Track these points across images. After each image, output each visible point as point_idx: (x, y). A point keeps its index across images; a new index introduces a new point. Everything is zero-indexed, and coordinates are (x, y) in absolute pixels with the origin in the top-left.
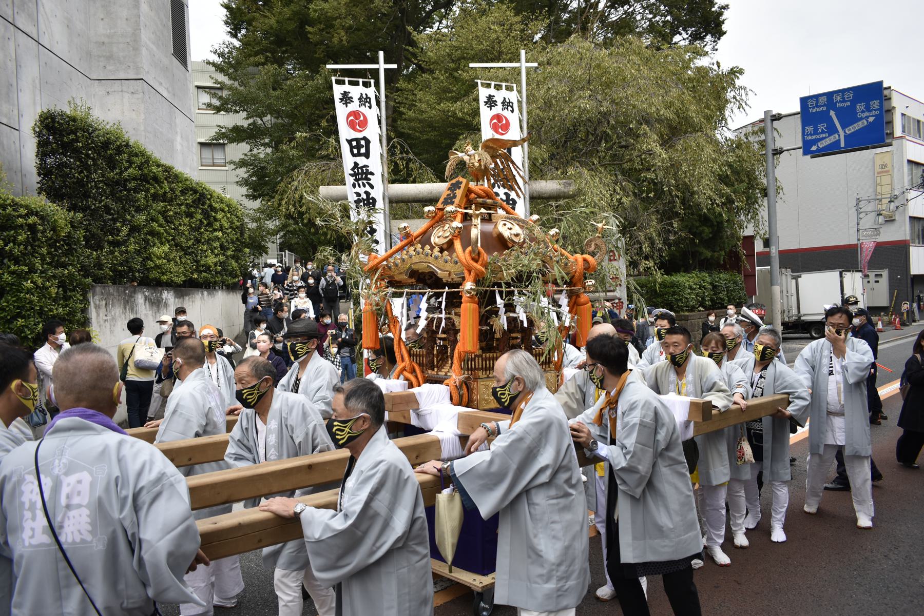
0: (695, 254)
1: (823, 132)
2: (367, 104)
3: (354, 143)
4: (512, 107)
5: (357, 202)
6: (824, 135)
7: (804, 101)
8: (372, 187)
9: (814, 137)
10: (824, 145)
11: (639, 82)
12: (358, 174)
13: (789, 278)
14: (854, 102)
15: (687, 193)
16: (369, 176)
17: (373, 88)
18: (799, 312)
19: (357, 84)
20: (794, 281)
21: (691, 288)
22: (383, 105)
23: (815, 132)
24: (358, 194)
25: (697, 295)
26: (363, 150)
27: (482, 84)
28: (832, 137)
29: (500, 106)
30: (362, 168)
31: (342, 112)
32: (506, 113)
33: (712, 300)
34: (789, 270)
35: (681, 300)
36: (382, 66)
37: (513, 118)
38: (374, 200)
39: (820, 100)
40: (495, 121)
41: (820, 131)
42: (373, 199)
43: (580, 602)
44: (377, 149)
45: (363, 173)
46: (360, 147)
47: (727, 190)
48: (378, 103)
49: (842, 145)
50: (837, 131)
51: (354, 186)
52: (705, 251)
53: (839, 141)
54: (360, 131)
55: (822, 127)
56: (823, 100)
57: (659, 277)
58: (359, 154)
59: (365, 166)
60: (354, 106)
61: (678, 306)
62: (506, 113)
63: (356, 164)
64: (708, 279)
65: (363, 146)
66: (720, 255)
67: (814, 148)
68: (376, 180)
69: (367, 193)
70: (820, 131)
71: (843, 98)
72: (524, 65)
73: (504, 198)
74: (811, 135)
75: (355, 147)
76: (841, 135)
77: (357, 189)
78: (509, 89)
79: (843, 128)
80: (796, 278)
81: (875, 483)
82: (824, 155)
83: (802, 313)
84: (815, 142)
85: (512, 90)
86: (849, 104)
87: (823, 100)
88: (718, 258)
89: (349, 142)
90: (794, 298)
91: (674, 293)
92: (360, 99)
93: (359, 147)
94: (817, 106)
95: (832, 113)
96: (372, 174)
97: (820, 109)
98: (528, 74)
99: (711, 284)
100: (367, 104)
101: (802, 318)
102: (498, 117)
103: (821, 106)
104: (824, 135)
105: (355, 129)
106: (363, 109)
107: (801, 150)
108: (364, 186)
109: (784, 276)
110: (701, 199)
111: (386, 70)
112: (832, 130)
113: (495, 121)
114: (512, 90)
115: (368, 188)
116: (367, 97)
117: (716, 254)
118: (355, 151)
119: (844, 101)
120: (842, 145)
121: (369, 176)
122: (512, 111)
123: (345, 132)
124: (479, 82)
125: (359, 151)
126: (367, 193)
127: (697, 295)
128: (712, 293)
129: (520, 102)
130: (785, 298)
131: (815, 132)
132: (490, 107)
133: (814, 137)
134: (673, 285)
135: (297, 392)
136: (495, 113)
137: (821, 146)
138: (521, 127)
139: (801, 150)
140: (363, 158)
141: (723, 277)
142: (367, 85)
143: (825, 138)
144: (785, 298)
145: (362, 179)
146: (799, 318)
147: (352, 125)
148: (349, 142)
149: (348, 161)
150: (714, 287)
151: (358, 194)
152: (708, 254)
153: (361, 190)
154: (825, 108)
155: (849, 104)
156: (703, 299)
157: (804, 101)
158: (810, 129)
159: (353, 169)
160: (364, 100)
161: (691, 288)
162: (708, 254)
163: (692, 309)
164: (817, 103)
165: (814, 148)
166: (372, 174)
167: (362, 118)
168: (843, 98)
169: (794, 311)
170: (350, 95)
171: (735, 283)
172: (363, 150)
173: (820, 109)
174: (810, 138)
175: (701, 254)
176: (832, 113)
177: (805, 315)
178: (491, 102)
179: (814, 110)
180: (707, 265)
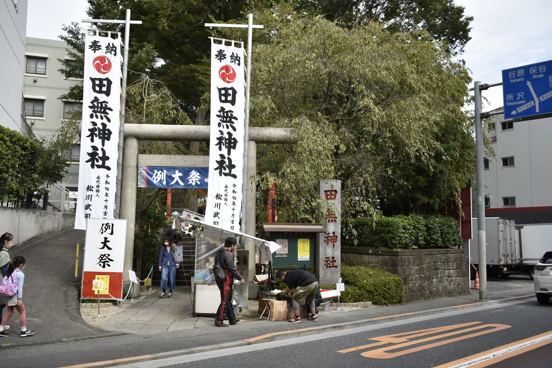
0: (414, 200)
1: (521, 99)
2: (113, 52)
3: (97, 82)
4: (239, 61)
6: (522, 102)
7: (505, 73)
9: (514, 103)
10: (522, 110)
11: (368, 48)
13: (513, 228)
14: (547, 74)
15: (399, 146)
16: (233, 120)
17: (120, 38)
18: (521, 256)
19: (106, 35)
20: (518, 231)
21: (404, 228)
22: (126, 53)
23: (515, 99)
24: (222, 133)
25: (411, 235)
26: (230, 98)
27: (214, 40)
28: (529, 104)
29: (104, 49)
30: (101, 103)
31: (216, 65)
32: (234, 66)
33: (425, 240)
34: (513, 222)
35: (395, 238)
36: (128, 22)
37: (239, 70)
39: (519, 72)
40: (224, 71)
41: (519, 98)
42: (234, 139)
44: (117, 90)
45: (102, 107)
46: (228, 95)
47: (438, 145)
48: (122, 53)
49: (537, 110)
50: (533, 99)
52: (422, 197)
53: (534, 107)
54: (104, 73)
55: (520, 95)
56: (521, 73)
57: (376, 216)
58: (226, 101)
59: (230, 111)
60: (227, 61)
61: (392, 244)
62: (234, 66)
63: (96, 99)
64: (423, 222)
65: (230, 95)
66: (436, 202)
67: (514, 113)
68: (239, 124)
69: (104, 125)
70: (519, 98)
71: (538, 71)
72: (251, 26)
73: (101, 127)
74: (511, 101)
76: (536, 102)
77: (94, 119)
78: (237, 45)
79: (538, 96)
80: (519, 228)
82: (524, 119)
83: (524, 257)
84: (515, 107)
85: (240, 47)
86: (542, 75)
87: (521, 73)
88: (434, 204)
89: (93, 80)
90: (517, 245)
91: (389, 232)
92: (107, 47)
93: (226, 95)
94: (516, 77)
95: (529, 84)
96: (236, 118)
97: (519, 80)
98: (253, 33)
99: (426, 226)
100: (113, 52)
101: (524, 262)
102: (227, 68)
103: (519, 77)
104: (522, 102)
105: (99, 71)
106: (108, 55)
107: (503, 115)
108: (102, 118)
109: (508, 227)
110: (412, 152)
111: (131, 25)
112: (529, 98)
113: (224, 71)
114: (240, 47)
116: (113, 46)
117: (432, 201)
119: (538, 73)
120: (537, 110)
121: (233, 120)
122: (239, 64)
123: (216, 82)
124: (212, 39)
125: (226, 98)
127: (411, 235)
128: (426, 234)
129: (246, 57)
130: (509, 245)
131: (515, 99)
132: (220, 60)
133: (514, 103)
134: (388, 224)
136: (99, 55)
137: (519, 111)
138: (246, 78)
139: (503, 115)
140: (104, 95)
141: (437, 221)
142: (114, 36)
143: (523, 104)
144: (509, 245)
146: (522, 261)
147: (223, 77)
148: (220, 90)
149: (215, 105)
150: (429, 229)
151: (94, 124)
152: (426, 200)
153: (99, 122)
154: (523, 79)
155: (542, 75)
156: (417, 238)
157: (505, 73)
158: (510, 97)
159: (92, 102)
160: (111, 49)
161: (404, 228)
162: (426, 200)
163: (406, 246)
164: (516, 75)
165: (514, 113)
166: (236, 118)
167: (231, 72)
168: (538, 71)
169: (518, 256)
170: (99, 44)
171: (450, 226)
172: (230, 98)
173: (519, 80)
174: (510, 104)
175: (418, 199)
176: (529, 84)
177: (526, 259)
178: (221, 55)
179: (514, 81)
180: (427, 210)
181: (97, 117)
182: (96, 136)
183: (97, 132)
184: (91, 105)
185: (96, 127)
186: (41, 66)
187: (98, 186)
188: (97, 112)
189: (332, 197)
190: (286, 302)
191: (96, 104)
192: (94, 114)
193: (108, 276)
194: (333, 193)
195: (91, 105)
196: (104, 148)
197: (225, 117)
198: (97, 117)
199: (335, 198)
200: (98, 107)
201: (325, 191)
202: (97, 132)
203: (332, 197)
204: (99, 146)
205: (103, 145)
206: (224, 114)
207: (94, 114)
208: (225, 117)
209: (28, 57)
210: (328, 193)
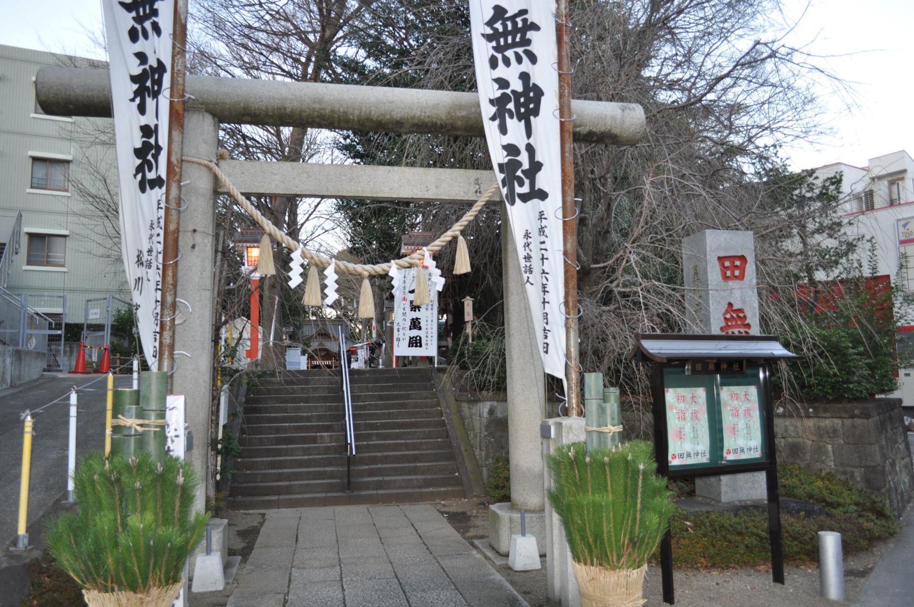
5: (500, 103)
8: (533, 59)
12: (505, 34)
24: (502, 83)
26: (738, 263)
30: (513, 18)
38: (539, 93)
43: (658, 360)
51: (493, 63)
69: (525, 77)
75: (733, 273)
77: (502, 71)
81: (856, 564)
89: (157, 29)
96: (535, 27)
115: (526, 66)
118: (729, 273)
126: (525, 77)
135: (421, 346)
145: (514, 45)
151: (502, 83)
153: (511, 74)
159: (490, 23)
181: (507, 62)
182: (512, 117)
183: (511, 106)
184: (489, 31)
185: (508, 91)
186: (57, 173)
187: (542, 230)
188: (508, 47)
189: (737, 273)
190: (757, 455)
191: (499, 26)
192: (499, 56)
193: (586, 375)
194: (738, 263)
195: (489, 31)
196: (531, 141)
197: (510, 33)
198: (507, 62)
199: (741, 277)
200: (505, 34)
201: (720, 259)
202: (511, 106)
203: (737, 273)
204: (521, 143)
205: (529, 133)
206: (505, 26)
207: (499, 56)
208: (510, 33)
209: (35, 159)
210: (727, 264)
